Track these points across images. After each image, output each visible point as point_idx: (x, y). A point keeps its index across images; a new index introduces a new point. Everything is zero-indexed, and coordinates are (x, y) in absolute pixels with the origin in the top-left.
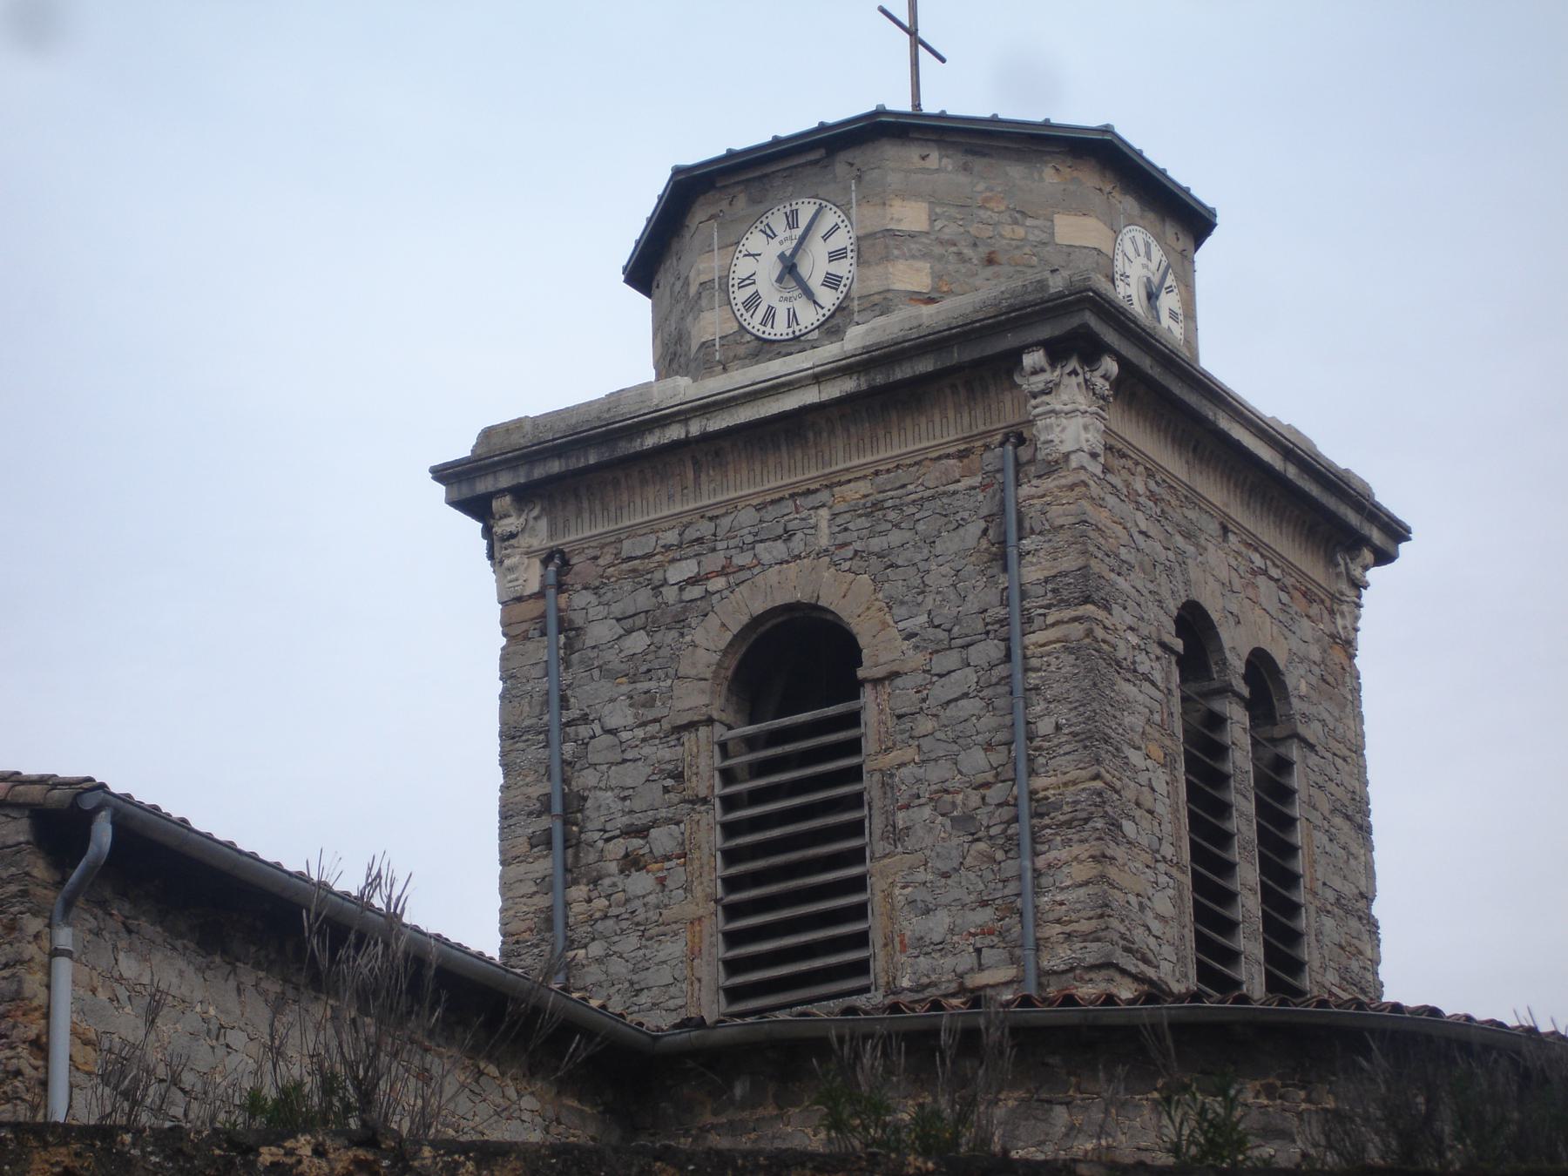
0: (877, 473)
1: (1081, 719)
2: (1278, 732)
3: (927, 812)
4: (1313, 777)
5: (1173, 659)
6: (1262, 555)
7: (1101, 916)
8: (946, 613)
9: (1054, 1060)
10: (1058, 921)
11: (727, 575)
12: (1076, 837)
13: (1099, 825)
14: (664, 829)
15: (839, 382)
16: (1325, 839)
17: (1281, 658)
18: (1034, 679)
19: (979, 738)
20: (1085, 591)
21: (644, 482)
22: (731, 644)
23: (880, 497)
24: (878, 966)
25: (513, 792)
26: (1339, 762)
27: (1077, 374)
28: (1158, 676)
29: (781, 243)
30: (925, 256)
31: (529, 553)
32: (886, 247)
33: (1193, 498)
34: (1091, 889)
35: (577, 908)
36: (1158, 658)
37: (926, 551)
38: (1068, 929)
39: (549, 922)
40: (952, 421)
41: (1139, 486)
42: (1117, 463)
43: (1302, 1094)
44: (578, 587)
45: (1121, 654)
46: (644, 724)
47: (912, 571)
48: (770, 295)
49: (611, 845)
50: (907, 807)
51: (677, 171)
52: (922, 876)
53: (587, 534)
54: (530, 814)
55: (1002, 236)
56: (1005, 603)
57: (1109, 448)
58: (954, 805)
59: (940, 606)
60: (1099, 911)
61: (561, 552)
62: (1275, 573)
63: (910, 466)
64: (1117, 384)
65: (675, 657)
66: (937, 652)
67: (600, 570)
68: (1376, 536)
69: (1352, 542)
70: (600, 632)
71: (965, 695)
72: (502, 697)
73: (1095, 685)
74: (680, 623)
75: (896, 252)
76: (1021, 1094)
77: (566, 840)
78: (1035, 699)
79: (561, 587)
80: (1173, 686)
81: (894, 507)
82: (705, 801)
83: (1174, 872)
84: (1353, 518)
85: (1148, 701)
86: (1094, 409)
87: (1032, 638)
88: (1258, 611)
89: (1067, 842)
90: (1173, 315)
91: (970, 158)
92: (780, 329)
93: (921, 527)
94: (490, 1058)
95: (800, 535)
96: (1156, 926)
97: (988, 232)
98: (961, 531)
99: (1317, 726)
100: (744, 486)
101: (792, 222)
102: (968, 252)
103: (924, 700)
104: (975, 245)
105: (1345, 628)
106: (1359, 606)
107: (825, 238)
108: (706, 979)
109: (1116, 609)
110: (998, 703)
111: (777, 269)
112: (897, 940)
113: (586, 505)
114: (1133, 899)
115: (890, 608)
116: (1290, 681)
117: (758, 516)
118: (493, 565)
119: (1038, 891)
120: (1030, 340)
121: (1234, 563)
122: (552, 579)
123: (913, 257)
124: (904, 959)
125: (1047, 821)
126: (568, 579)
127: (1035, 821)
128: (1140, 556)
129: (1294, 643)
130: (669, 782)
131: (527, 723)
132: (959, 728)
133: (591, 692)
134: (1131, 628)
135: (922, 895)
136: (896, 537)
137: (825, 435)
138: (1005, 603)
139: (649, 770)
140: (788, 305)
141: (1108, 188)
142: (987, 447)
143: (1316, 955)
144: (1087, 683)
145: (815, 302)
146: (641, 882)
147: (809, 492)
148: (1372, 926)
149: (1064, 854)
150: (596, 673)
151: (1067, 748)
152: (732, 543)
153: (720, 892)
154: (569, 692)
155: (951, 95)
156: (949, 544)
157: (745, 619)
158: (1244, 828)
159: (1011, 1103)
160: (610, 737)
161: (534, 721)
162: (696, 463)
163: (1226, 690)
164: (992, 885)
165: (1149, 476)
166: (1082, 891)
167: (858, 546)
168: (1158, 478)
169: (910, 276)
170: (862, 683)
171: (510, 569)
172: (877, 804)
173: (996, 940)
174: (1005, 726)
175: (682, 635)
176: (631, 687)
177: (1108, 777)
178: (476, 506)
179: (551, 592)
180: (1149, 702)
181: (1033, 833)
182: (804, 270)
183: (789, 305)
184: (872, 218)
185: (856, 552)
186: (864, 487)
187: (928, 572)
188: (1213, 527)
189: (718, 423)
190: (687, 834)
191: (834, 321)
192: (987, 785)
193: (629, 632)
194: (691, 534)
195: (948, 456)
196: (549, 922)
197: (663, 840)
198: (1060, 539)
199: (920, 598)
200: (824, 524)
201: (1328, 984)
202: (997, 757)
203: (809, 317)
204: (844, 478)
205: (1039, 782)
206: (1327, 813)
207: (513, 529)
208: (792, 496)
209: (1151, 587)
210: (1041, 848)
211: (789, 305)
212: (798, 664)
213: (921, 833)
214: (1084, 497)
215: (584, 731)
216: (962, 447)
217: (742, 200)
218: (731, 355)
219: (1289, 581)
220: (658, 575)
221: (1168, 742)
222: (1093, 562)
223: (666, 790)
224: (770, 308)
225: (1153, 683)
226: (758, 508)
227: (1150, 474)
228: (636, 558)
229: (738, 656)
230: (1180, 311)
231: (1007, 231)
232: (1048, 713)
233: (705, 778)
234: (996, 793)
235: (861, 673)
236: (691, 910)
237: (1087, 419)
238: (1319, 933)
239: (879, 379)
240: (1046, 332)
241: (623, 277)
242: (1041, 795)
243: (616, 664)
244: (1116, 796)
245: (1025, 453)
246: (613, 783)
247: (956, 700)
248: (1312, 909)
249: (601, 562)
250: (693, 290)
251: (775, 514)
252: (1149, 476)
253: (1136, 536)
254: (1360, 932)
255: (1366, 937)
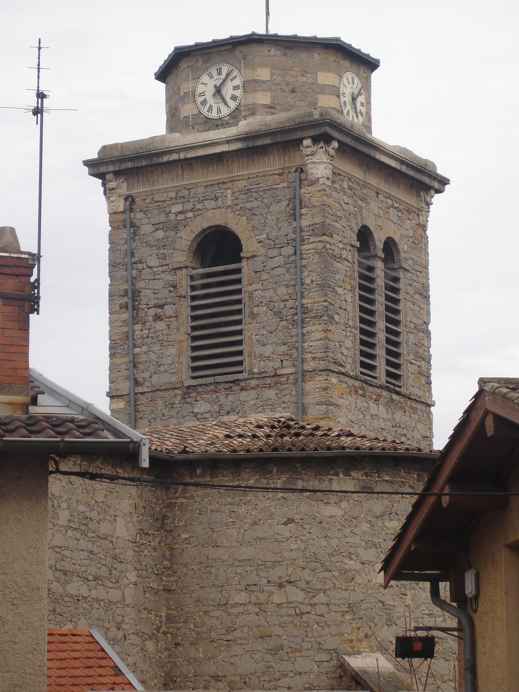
0: (249, 178)
1: (321, 279)
2: (395, 266)
3: (265, 309)
4: (407, 281)
5: (356, 249)
6: (392, 200)
7: (325, 352)
8: (274, 234)
9: (298, 465)
10: (310, 352)
11: (193, 211)
12: (317, 322)
13: (326, 319)
14: (169, 306)
15: (235, 144)
16: (411, 305)
17: (397, 239)
18: (304, 262)
19: (284, 283)
20: (324, 231)
21: (163, 172)
22: (195, 238)
23: (250, 187)
24: (246, 363)
25: (114, 287)
26: (418, 273)
27: (323, 148)
28: (349, 258)
29: (215, 80)
30: (269, 90)
31: (119, 196)
32: (255, 87)
33: (366, 185)
34: (322, 342)
35: (138, 333)
36: (350, 250)
37: (267, 210)
38: (313, 356)
39: (127, 336)
40: (277, 161)
41: (345, 186)
42: (337, 178)
43: (377, 475)
44: (138, 210)
45: (335, 253)
46: (162, 266)
47: (261, 217)
48: (211, 101)
49: (150, 310)
50: (258, 306)
51: (176, 49)
52: (262, 332)
53: (141, 190)
54: (120, 296)
55: (297, 81)
56: (294, 233)
57: (334, 173)
58: (274, 307)
59: (272, 232)
60: (325, 350)
61: (132, 196)
62: (396, 205)
63: (261, 176)
64: (337, 150)
65: (174, 242)
66: (270, 249)
67: (146, 205)
68: (436, 185)
69: (427, 188)
70: (146, 229)
71: (280, 266)
72: (109, 250)
73: (326, 267)
74: (176, 228)
75: (258, 89)
76: (288, 476)
77: (133, 307)
78: (304, 270)
79: (131, 210)
80: (355, 260)
81: (255, 192)
82: (184, 297)
83: (353, 330)
84: (427, 180)
85: (346, 268)
86: (329, 161)
87: (304, 247)
88: (389, 222)
89: (314, 324)
90: (362, 104)
91: (286, 50)
92: (214, 115)
93: (265, 200)
94: (120, 468)
95: (220, 199)
96: (345, 352)
97: (293, 79)
98: (280, 204)
99: (410, 262)
100: (200, 178)
101: (219, 73)
102: (285, 88)
103: (265, 267)
104: (288, 85)
105: (423, 220)
106: (428, 212)
107: (232, 80)
108: (184, 363)
109: (335, 236)
110: (291, 270)
111: (214, 90)
112: (253, 354)
113: (141, 179)
114: (337, 344)
115: (253, 231)
116: (400, 247)
117: (205, 190)
118: (106, 198)
119: (303, 341)
120: (306, 136)
121: (380, 206)
122: (128, 207)
123: (264, 90)
124: (255, 362)
125: (307, 316)
126: (134, 207)
127: (303, 315)
128: (344, 213)
129: (403, 231)
130: (171, 289)
131: (118, 261)
132: (277, 278)
133: (142, 252)
134: (340, 242)
135: (262, 339)
136: (255, 204)
137: (230, 161)
138: (294, 233)
139: (164, 283)
140: (217, 105)
141: (338, 60)
142: (290, 172)
143: (406, 349)
144: (323, 266)
145: (227, 105)
146: (161, 325)
147: (224, 183)
148: (428, 334)
149: (313, 328)
150: (144, 244)
151: (315, 289)
152: (196, 199)
153: (190, 332)
154: (134, 251)
155: (281, 28)
156: (275, 208)
157: (200, 230)
158: (380, 308)
159: (284, 479)
160: (150, 270)
161: (122, 260)
162: (182, 166)
163: (375, 256)
164: (287, 338)
165: (349, 180)
166: (319, 342)
167: (242, 205)
168: (352, 180)
169: (263, 98)
170: (242, 258)
171: (113, 202)
172: (247, 304)
173: (288, 357)
174: (293, 279)
175: (177, 233)
176: (158, 251)
177: (329, 300)
178: (100, 176)
179: (128, 212)
180: (346, 270)
181: (302, 320)
182: (223, 92)
183: (218, 105)
184: (250, 75)
185: (241, 208)
186: (244, 183)
187: (267, 218)
188: (373, 194)
189: (191, 155)
190: (178, 309)
191: (234, 114)
192: (287, 300)
193: (157, 230)
194: (180, 194)
195: (275, 174)
196: (127, 336)
197: (169, 310)
198: (315, 211)
199: (264, 228)
200: (229, 196)
201: (410, 360)
202: (291, 290)
203: (225, 111)
204: (237, 179)
205: (305, 301)
206: (412, 295)
207: (114, 187)
208: (218, 183)
209: (348, 223)
210: (305, 325)
211: (218, 105)
212: (219, 247)
213: (262, 316)
214: (324, 195)
215: (140, 266)
216: (280, 172)
217: (200, 62)
218: (196, 123)
219: (401, 207)
220: (168, 209)
221: (352, 282)
222: (327, 220)
223: (170, 292)
224: (211, 106)
225: (348, 261)
226: (205, 187)
227: (349, 179)
228: (160, 201)
229: (197, 243)
230: (365, 102)
231: (300, 79)
232: (309, 276)
233: (184, 288)
234: (290, 304)
235: (242, 255)
236: (179, 337)
237: (326, 165)
238: (407, 341)
239: (251, 145)
240: (312, 133)
241: (154, 77)
242: (305, 306)
243: (152, 242)
244: (333, 307)
245: (303, 176)
246: (151, 287)
247: (276, 267)
248: (405, 333)
249: (147, 201)
250: (182, 94)
251: (211, 190)
252: (349, 180)
253: (343, 205)
254: (423, 337)
255: (426, 339)
